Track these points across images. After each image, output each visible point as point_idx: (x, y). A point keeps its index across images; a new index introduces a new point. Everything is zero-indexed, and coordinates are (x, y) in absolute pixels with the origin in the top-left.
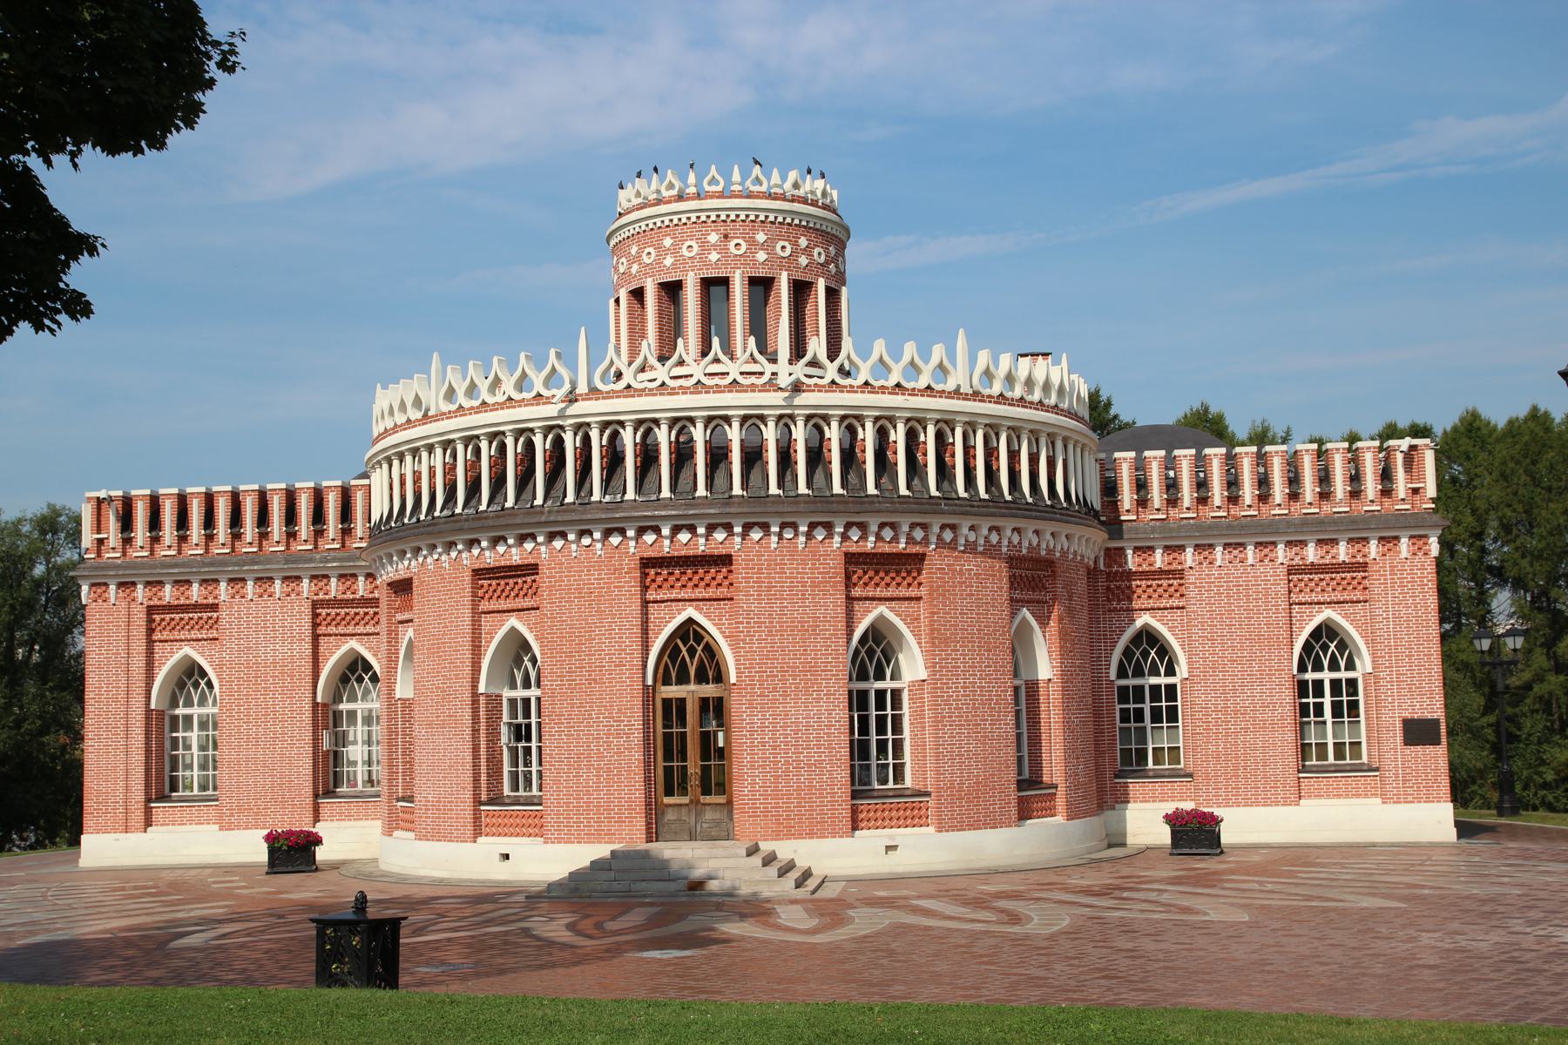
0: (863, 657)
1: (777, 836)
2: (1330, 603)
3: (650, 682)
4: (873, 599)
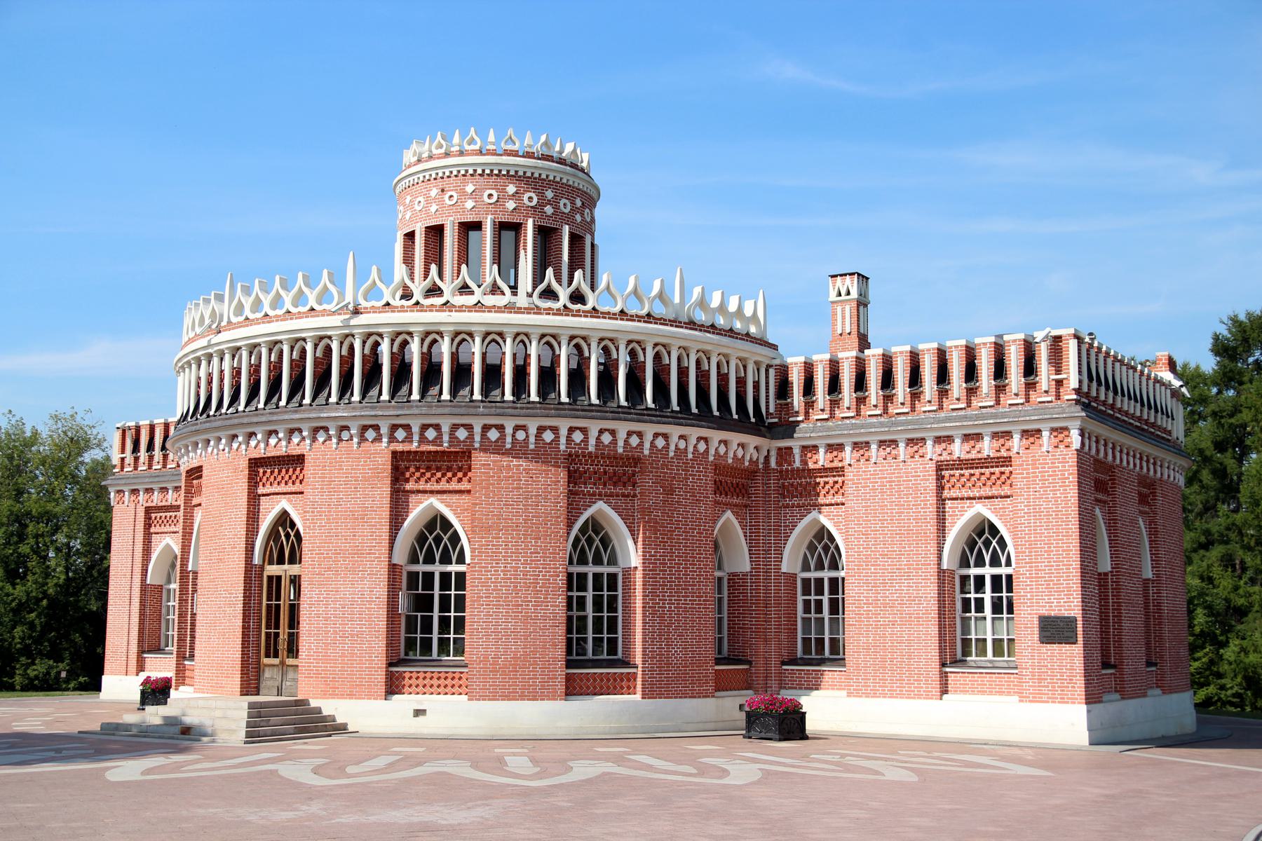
0: (994, 547)
1: (325, 695)
2: (980, 498)
3: (257, 560)
4: (425, 492)
